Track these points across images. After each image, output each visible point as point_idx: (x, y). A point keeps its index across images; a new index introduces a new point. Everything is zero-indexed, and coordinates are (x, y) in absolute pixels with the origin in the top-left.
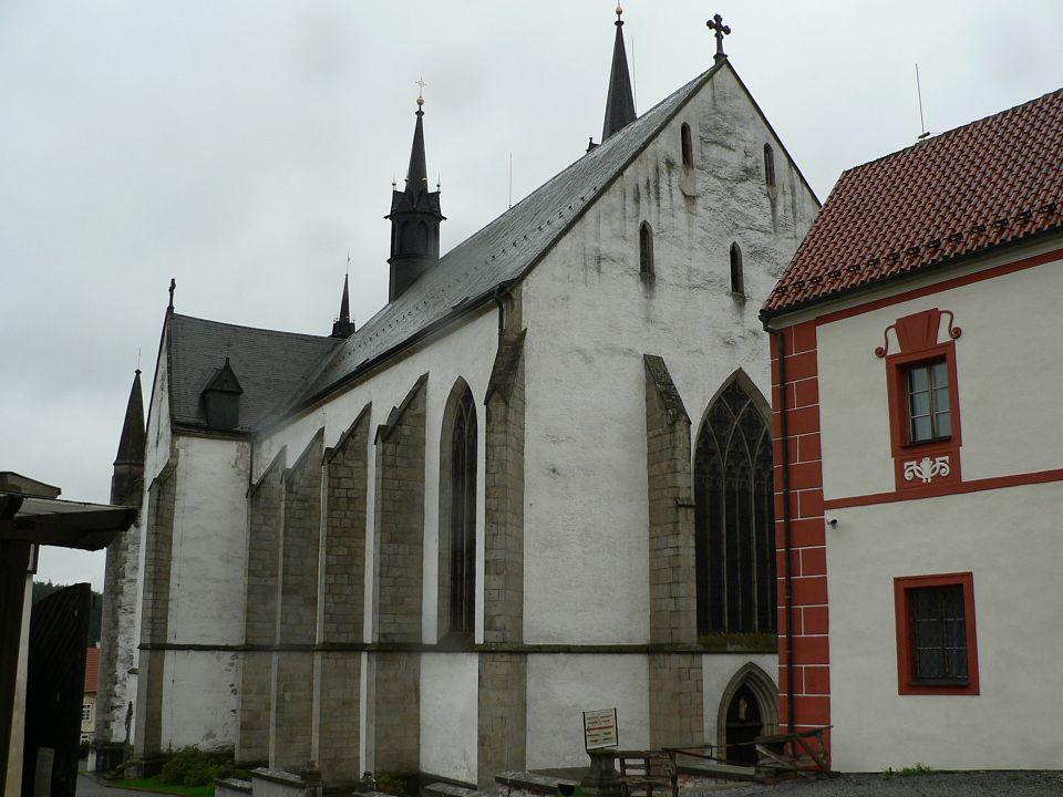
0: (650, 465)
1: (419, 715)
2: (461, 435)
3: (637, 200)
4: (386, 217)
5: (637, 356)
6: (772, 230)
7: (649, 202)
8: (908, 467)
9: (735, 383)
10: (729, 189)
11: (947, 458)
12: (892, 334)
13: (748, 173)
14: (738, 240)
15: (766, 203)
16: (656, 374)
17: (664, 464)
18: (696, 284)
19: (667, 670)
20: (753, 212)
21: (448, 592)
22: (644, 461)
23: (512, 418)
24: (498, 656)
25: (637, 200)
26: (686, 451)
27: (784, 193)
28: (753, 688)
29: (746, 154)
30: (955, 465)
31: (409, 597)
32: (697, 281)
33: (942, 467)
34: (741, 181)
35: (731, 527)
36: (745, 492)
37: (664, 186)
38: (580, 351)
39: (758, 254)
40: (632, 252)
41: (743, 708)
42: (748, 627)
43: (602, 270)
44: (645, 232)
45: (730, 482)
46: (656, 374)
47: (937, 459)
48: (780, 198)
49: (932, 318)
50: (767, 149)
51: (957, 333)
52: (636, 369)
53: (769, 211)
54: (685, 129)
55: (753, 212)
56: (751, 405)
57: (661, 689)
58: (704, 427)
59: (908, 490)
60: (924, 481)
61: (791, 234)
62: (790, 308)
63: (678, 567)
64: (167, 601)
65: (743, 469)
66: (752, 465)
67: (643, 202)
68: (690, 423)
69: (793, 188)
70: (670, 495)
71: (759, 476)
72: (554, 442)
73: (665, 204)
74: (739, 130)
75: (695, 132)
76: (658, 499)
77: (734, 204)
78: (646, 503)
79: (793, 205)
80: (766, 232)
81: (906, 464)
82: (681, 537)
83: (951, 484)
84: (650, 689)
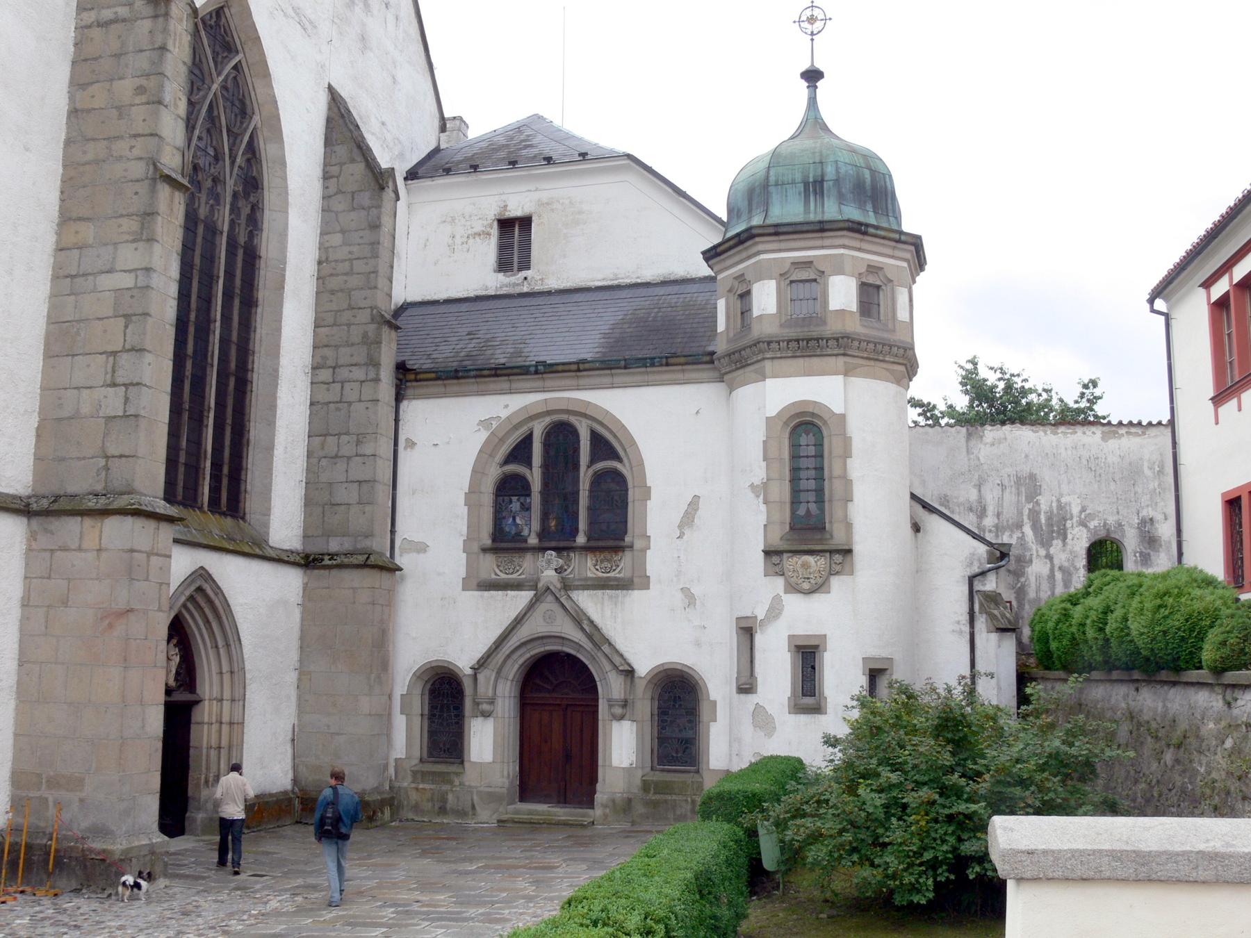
0: (78, 84)
17: (125, 87)
19: (91, 556)
22: (62, 73)
28: (196, 627)
57: (65, 603)
63: (146, 314)
64: (782, 491)
70: (136, 152)
76: (97, 162)
78: (56, 168)
82: (157, 248)
84: (26, 603)
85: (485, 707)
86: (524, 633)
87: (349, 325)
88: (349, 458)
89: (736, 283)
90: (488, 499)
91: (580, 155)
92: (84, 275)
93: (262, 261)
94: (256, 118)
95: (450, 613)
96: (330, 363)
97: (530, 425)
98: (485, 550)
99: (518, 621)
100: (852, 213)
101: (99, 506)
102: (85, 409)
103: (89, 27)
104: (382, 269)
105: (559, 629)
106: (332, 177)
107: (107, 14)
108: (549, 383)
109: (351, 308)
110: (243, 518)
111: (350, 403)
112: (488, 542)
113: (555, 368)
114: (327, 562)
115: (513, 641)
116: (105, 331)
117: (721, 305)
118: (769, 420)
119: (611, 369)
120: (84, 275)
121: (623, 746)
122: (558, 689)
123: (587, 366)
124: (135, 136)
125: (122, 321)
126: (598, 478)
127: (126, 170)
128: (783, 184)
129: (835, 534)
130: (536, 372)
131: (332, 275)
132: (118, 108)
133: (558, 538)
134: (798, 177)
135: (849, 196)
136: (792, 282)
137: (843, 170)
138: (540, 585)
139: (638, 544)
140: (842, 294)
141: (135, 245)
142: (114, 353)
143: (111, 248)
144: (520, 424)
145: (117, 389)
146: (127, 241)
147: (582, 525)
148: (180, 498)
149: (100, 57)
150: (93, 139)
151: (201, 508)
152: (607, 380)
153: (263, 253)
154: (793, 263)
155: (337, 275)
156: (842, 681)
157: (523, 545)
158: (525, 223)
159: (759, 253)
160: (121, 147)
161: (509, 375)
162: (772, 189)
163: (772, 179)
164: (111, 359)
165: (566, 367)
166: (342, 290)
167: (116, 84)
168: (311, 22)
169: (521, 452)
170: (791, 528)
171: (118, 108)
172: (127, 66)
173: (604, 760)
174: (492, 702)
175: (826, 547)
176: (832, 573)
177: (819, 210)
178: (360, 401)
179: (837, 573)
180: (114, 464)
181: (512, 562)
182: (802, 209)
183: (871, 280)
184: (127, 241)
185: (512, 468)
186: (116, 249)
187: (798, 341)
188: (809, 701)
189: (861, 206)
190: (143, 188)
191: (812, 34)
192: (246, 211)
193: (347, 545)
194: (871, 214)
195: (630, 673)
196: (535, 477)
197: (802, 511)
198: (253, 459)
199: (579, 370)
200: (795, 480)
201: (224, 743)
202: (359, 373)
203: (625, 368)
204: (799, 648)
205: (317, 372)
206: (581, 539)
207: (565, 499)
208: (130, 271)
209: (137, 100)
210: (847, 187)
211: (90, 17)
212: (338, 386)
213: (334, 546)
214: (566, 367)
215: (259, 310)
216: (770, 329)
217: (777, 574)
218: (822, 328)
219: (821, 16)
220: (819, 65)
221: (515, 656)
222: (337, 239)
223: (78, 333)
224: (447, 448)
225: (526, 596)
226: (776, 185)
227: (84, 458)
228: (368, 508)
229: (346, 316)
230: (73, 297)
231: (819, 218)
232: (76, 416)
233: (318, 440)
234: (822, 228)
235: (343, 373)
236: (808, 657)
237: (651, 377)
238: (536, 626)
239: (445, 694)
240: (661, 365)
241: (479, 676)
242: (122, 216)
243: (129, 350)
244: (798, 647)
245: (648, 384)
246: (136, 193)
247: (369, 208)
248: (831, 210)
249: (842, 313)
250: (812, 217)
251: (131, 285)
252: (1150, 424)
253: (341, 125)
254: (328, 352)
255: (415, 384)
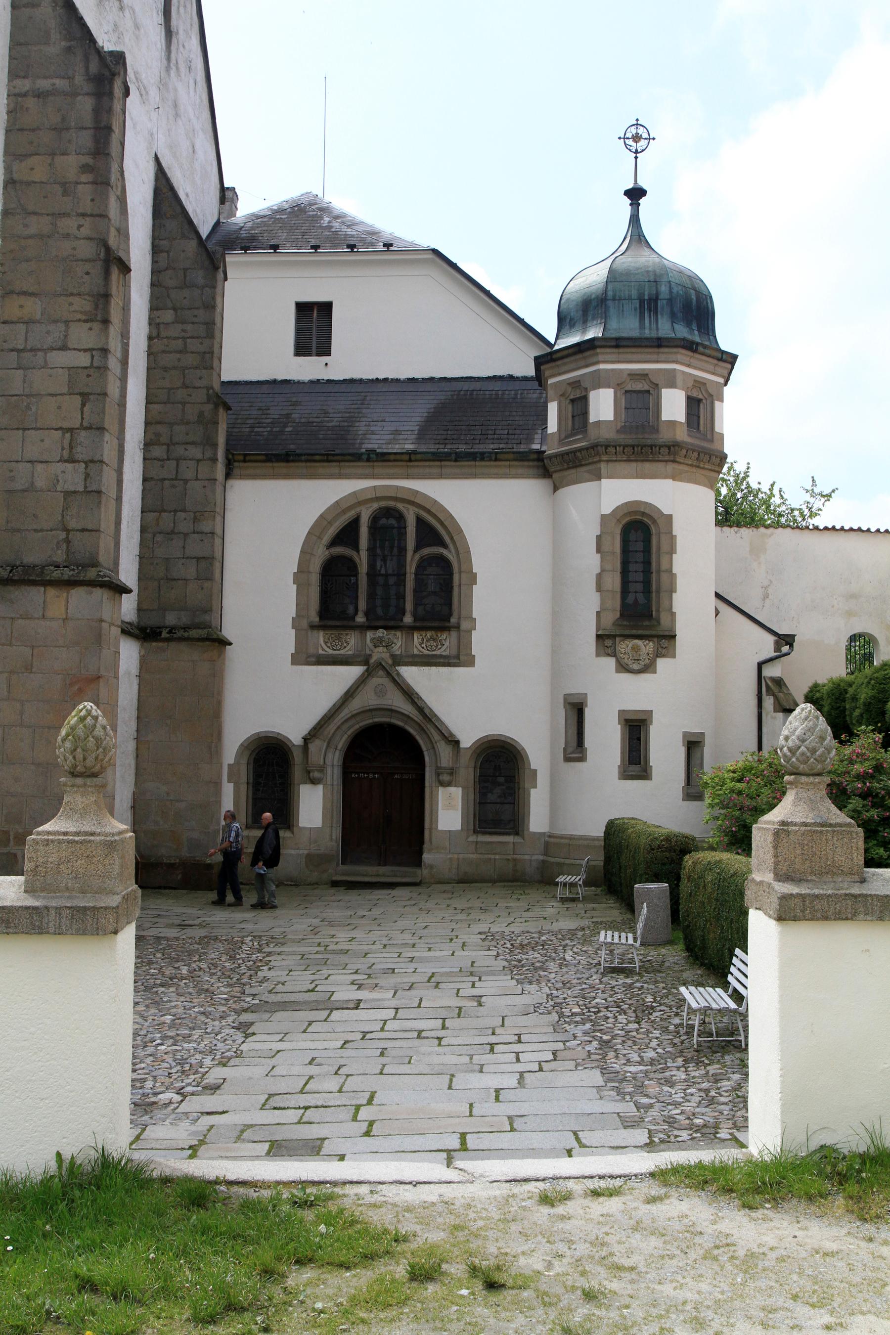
64: (614, 582)
70: (84, 231)
76: (40, 236)
85: (316, 775)
86: (356, 705)
87: (184, 404)
88: (186, 535)
89: (569, 389)
90: (315, 579)
91: (385, 245)
92: (31, 350)
95: (279, 685)
96: (164, 439)
97: (358, 509)
98: (313, 627)
99: (349, 695)
100: (682, 331)
101: (66, 577)
102: (40, 483)
103: (25, 95)
104: (216, 350)
105: (389, 702)
106: (162, 251)
107: (44, 84)
108: (378, 471)
109: (185, 386)
111: (186, 481)
112: (316, 619)
113: (387, 457)
114: (164, 634)
115: (345, 713)
116: (59, 408)
117: (553, 409)
118: (603, 517)
119: (441, 461)
120: (31, 350)
121: (448, 811)
122: (386, 760)
123: (419, 457)
124: (84, 215)
125: (78, 400)
126: (422, 566)
127: (74, 249)
128: (620, 300)
129: (662, 621)
130: (368, 460)
131: (164, 352)
132: (64, 185)
133: (386, 617)
134: (634, 293)
135: (680, 315)
136: (626, 392)
137: (675, 291)
138: (372, 661)
139: (464, 625)
140: (673, 406)
141: (88, 325)
142: (71, 430)
143: (62, 326)
144: (350, 508)
145: (76, 465)
146: (79, 320)
147: (409, 606)
149: (38, 129)
150: (35, 213)
152: (435, 471)
154: (629, 375)
155: (170, 352)
156: (665, 752)
157: (351, 623)
158: (326, 308)
159: (598, 363)
160: (69, 224)
161: (339, 461)
162: (610, 303)
163: (610, 294)
164: (68, 435)
165: (398, 457)
166: (174, 368)
167: (59, 160)
169: (347, 534)
170: (621, 615)
171: (64, 185)
172: (69, 141)
173: (431, 824)
174: (322, 769)
175: (654, 633)
176: (658, 655)
177: (654, 326)
178: (197, 479)
179: (663, 656)
180: (76, 537)
181: (339, 639)
182: (637, 324)
183: (695, 394)
184: (79, 320)
185: (338, 550)
186: (67, 327)
187: (633, 446)
188: (635, 769)
189: (688, 325)
190: (97, 269)
191: (636, 152)
193: (185, 619)
194: (696, 332)
195: (455, 743)
196: (362, 560)
197: (630, 599)
199: (410, 460)
200: (625, 572)
202: (195, 452)
203: (456, 461)
204: (627, 721)
205: (151, 448)
206: (408, 619)
207: (389, 585)
208: (85, 350)
209: (84, 178)
210: (678, 306)
211: (25, 85)
212: (174, 463)
213: (171, 619)
214: (398, 457)
216: (608, 435)
217: (608, 655)
218: (654, 436)
219: (645, 135)
220: (643, 183)
221: (344, 727)
222: (168, 316)
223: (28, 408)
224: (272, 529)
225: (355, 671)
226: (614, 299)
227: (42, 530)
228: (207, 584)
229: (181, 394)
230: (21, 372)
231: (654, 335)
232: (31, 488)
233: (152, 516)
234: (659, 343)
235: (180, 451)
236: (636, 729)
237: (513, 471)
238: (367, 699)
239: (272, 764)
240: (491, 460)
241: (310, 746)
242: (72, 294)
243: (87, 428)
244: (627, 721)
245: (474, 476)
246: (87, 273)
247: (203, 287)
248: (665, 328)
249: (673, 424)
250: (647, 333)
251: (87, 363)
252: (842, 529)
253: (165, 194)
254: (162, 429)
255: (242, 464)
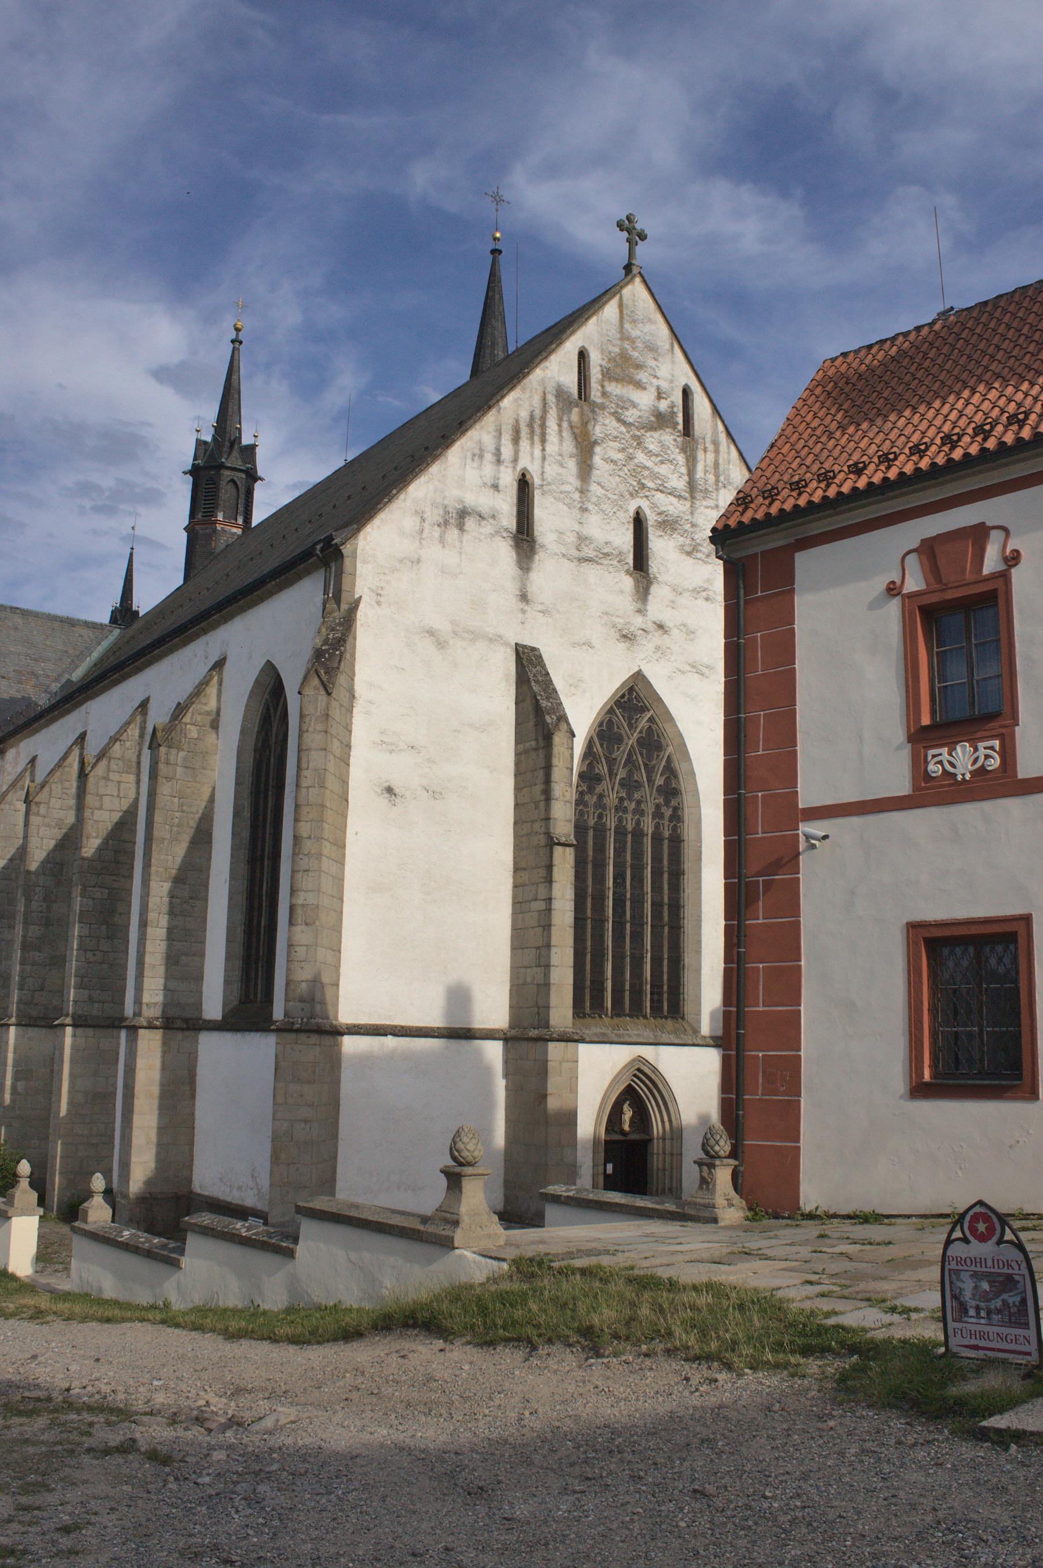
1: (193, 1114)
2: (266, 741)
3: (516, 440)
4: (185, 473)
5: (506, 644)
6: (687, 495)
7: (532, 444)
8: (934, 756)
9: (631, 690)
10: (635, 437)
11: (996, 743)
12: (912, 561)
13: (661, 420)
14: (645, 505)
15: (681, 459)
16: (528, 665)
18: (586, 554)
20: (664, 470)
21: (239, 950)
23: (336, 712)
24: (303, 1037)
25: (516, 440)
26: (566, 772)
27: (705, 450)
28: (641, 1090)
29: (659, 397)
30: (1008, 754)
31: (187, 955)
32: (591, 553)
33: (987, 757)
34: (651, 428)
35: (619, 876)
36: (638, 834)
37: (552, 424)
38: (431, 633)
39: (669, 525)
40: (506, 506)
41: (628, 1114)
42: (636, 1010)
43: (466, 528)
44: (524, 485)
45: (620, 820)
46: (528, 665)
47: (981, 745)
48: (700, 455)
49: (979, 534)
50: (686, 393)
51: (1013, 559)
52: (505, 665)
53: (684, 470)
54: (582, 355)
55: (664, 470)
56: (651, 720)
58: (590, 745)
59: (930, 791)
60: (959, 778)
61: (711, 503)
62: (755, 525)
65: (639, 802)
66: (651, 800)
67: (524, 444)
68: (573, 735)
69: (716, 444)
71: (658, 814)
72: (391, 751)
73: (552, 447)
74: (651, 363)
75: (595, 359)
77: (641, 457)
79: (716, 465)
80: (679, 497)
81: (931, 752)
83: (1001, 783)
93: (686, 843)
94: (670, 749)
110: (683, 1018)
148: (627, 1011)
151: (645, 1017)
153: (686, 838)
168: (707, 667)
192: (668, 812)
198: (688, 977)
201: (667, 1167)
215: (686, 877)
